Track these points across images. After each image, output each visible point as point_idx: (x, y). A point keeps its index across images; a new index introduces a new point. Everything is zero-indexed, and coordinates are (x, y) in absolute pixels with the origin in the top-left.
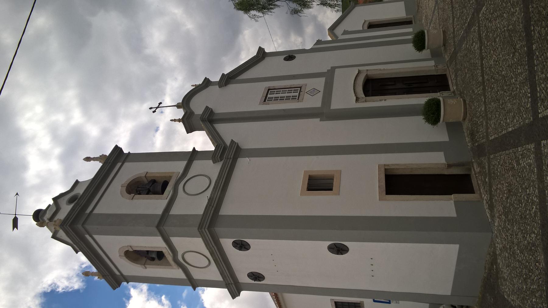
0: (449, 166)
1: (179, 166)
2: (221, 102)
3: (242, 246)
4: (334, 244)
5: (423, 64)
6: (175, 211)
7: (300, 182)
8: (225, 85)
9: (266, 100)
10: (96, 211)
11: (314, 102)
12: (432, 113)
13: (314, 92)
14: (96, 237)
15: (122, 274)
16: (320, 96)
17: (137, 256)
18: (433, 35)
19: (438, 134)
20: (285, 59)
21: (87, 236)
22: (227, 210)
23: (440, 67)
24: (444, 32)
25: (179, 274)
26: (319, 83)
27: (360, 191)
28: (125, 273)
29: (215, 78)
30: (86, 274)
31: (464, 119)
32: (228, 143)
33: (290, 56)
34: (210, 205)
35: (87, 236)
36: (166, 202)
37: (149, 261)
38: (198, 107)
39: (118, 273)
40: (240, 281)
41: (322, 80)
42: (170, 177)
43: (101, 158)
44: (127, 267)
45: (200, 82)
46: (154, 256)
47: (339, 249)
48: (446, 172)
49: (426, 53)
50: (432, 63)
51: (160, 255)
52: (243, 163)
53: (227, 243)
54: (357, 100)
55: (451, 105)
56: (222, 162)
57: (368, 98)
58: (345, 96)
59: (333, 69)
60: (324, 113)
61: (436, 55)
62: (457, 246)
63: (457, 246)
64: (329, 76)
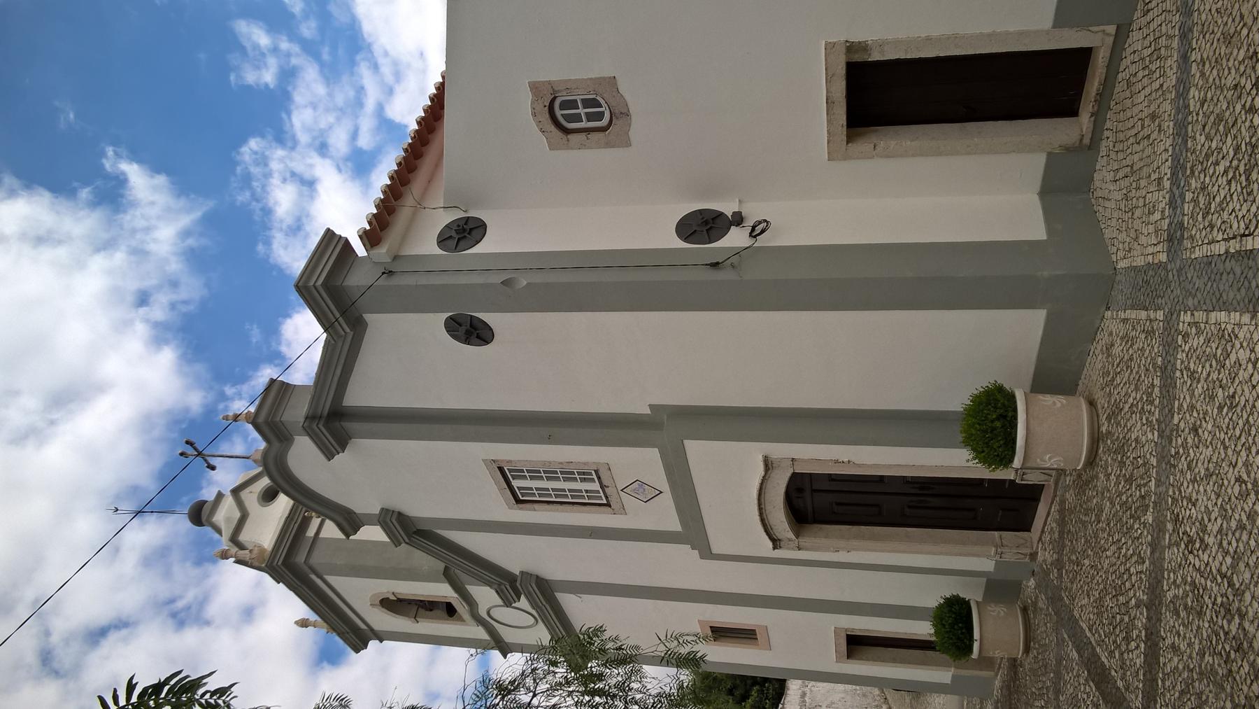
7: (817, 96)
14: (330, 579)
15: (372, 630)
17: (394, 605)
21: (313, 577)
25: (481, 633)
28: (376, 627)
30: (303, 623)
34: (332, 325)
35: (313, 577)
37: (421, 611)
39: (363, 626)
40: (357, 511)
44: (381, 620)
51: (450, 610)
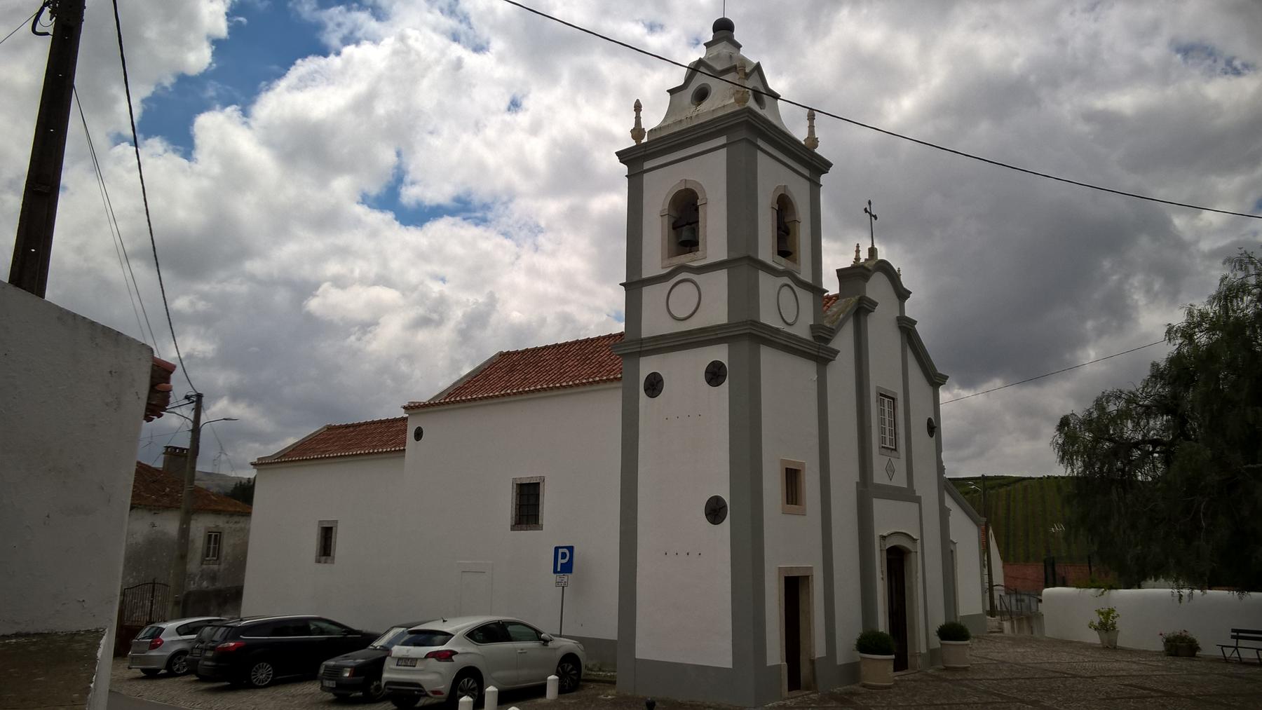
0: (812, 662)
1: (805, 275)
2: (881, 327)
3: (715, 374)
4: (725, 506)
5: (923, 636)
6: (763, 277)
7: (794, 458)
8: (900, 327)
9: (882, 395)
10: (760, 154)
11: (879, 477)
12: (869, 643)
13: (890, 471)
16: (886, 481)
18: (968, 653)
19: (845, 650)
20: (930, 420)
22: (769, 359)
23: (919, 661)
24: (966, 669)
26: (900, 481)
27: (789, 543)
29: (911, 309)
31: (864, 686)
32: (832, 345)
33: (933, 428)
36: (769, 262)
38: (877, 288)
41: (903, 484)
42: (795, 261)
43: (812, 140)
44: (662, 185)
45: (906, 283)
46: (685, 235)
47: (715, 511)
48: (803, 658)
49: (936, 642)
50: (924, 650)
52: (808, 369)
53: (720, 353)
54: (883, 538)
55: (880, 667)
56: (810, 339)
57: (885, 554)
58: (890, 519)
59: (917, 500)
60: (866, 491)
61: (933, 654)
62: (726, 662)
63: (726, 662)
64: (907, 494)
